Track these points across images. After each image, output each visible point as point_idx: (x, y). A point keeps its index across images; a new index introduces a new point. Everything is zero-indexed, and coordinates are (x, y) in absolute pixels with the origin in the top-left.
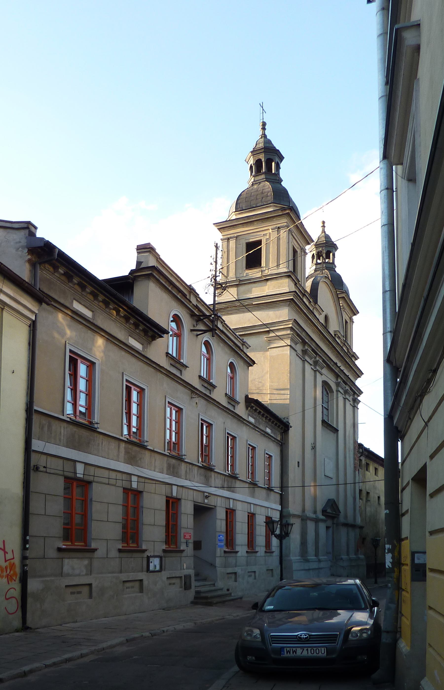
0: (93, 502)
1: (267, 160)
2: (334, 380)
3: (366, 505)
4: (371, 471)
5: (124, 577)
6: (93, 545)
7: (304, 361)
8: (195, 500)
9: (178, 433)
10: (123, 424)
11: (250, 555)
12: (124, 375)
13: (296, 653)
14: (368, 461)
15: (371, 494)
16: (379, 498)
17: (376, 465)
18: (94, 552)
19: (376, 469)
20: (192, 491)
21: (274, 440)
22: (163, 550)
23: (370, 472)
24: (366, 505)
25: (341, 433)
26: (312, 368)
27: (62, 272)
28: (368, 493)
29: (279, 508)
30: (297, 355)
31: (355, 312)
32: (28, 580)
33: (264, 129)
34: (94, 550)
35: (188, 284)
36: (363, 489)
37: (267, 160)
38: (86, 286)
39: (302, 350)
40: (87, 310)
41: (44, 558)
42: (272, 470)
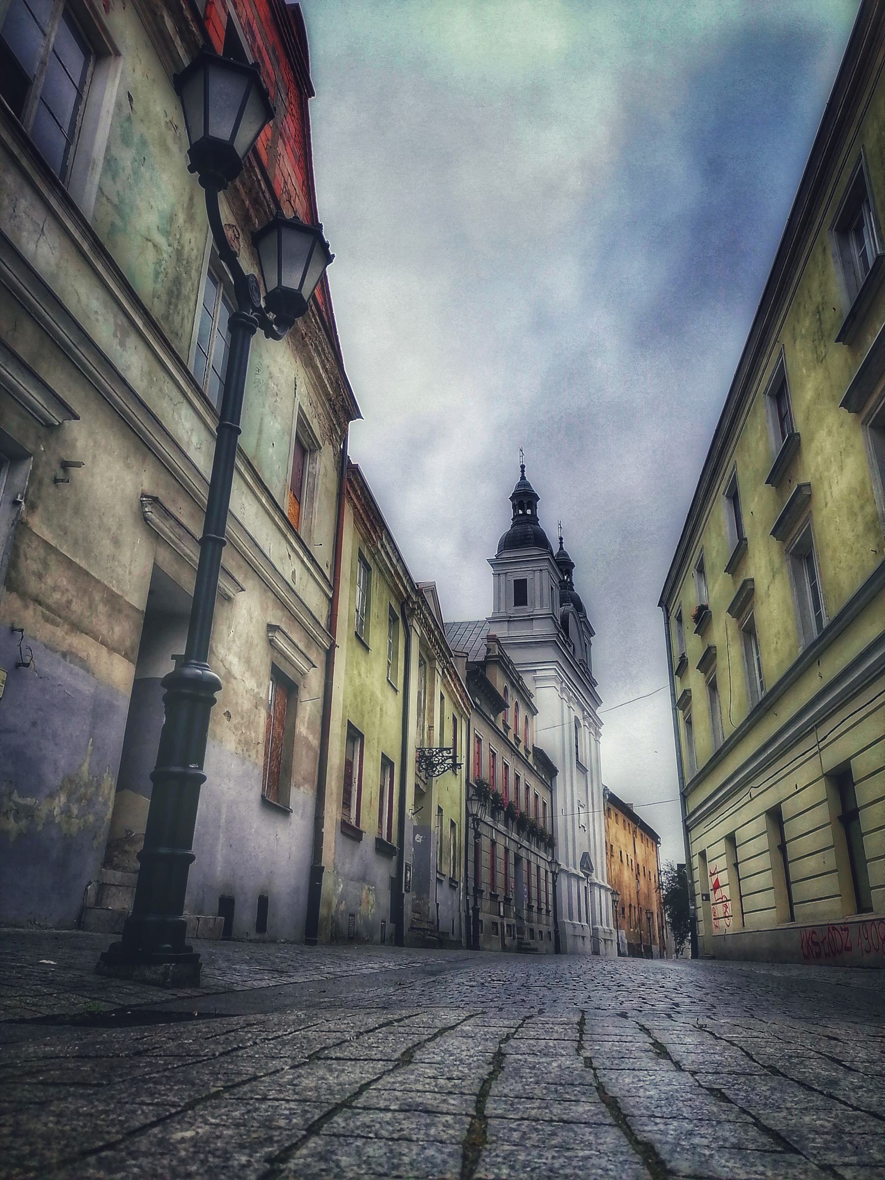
1: (524, 499)
21: (543, 782)
33: (523, 471)
37: (524, 499)
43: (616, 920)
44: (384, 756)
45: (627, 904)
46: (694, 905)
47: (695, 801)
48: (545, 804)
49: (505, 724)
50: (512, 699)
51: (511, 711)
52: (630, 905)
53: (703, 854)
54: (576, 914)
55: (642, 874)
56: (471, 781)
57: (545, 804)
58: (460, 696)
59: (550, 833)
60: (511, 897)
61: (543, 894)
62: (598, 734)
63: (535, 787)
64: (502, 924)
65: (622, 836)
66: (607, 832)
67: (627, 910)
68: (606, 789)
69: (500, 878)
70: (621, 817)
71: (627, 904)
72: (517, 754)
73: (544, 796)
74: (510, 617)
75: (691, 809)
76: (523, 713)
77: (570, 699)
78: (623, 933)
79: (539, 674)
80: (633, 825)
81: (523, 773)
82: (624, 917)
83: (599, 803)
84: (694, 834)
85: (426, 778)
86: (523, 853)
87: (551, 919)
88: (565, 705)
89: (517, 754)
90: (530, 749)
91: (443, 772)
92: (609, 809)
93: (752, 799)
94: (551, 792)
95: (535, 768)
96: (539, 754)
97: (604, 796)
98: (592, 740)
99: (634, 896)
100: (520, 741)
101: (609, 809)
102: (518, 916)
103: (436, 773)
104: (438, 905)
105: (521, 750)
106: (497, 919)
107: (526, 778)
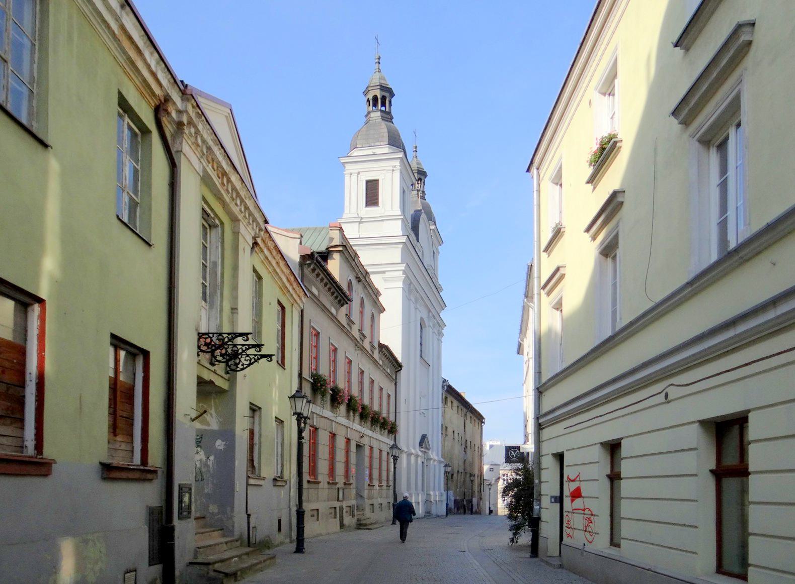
18: (319, 483)
21: (388, 376)
43: (447, 484)
44: (113, 336)
45: (456, 471)
46: (539, 505)
47: (553, 399)
48: (389, 396)
49: (348, 316)
50: (357, 293)
51: (356, 304)
52: (458, 471)
53: (560, 457)
54: (413, 486)
55: (469, 447)
56: (306, 375)
57: (389, 396)
58: (288, 280)
59: (393, 421)
60: (351, 481)
61: (384, 474)
62: (440, 334)
63: (381, 380)
64: (341, 509)
65: (454, 416)
66: (443, 416)
67: (455, 475)
68: (445, 381)
69: (340, 469)
70: (456, 403)
71: (456, 471)
72: (363, 349)
73: (388, 387)
74: (362, 218)
75: (546, 408)
76: (369, 308)
77: (416, 301)
78: (451, 493)
79: (387, 274)
80: (465, 410)
81: (368, 367)
82: (453, 481)
83: (439, 393)
84: (546, 433)
85: (227, 373)
86: (365, 441)
87: (391, 492)
88: (412, 306)
89: (363, 349)
90: (376, 345)
91: (249, 365)
92: (446, 398)
93: (669, 402)
94: (396, 384)
95: (381, 363)
96: (383, 348)
97: (443, 387)
98: (435, 339)
99: (461, 464)
100: (365, 337)
101: (446, 398)
102: (359, 496)
103: (240, 366)
104: (249, 516)
105: (367, 345)
106: (337, 504)
107: (371, 372)
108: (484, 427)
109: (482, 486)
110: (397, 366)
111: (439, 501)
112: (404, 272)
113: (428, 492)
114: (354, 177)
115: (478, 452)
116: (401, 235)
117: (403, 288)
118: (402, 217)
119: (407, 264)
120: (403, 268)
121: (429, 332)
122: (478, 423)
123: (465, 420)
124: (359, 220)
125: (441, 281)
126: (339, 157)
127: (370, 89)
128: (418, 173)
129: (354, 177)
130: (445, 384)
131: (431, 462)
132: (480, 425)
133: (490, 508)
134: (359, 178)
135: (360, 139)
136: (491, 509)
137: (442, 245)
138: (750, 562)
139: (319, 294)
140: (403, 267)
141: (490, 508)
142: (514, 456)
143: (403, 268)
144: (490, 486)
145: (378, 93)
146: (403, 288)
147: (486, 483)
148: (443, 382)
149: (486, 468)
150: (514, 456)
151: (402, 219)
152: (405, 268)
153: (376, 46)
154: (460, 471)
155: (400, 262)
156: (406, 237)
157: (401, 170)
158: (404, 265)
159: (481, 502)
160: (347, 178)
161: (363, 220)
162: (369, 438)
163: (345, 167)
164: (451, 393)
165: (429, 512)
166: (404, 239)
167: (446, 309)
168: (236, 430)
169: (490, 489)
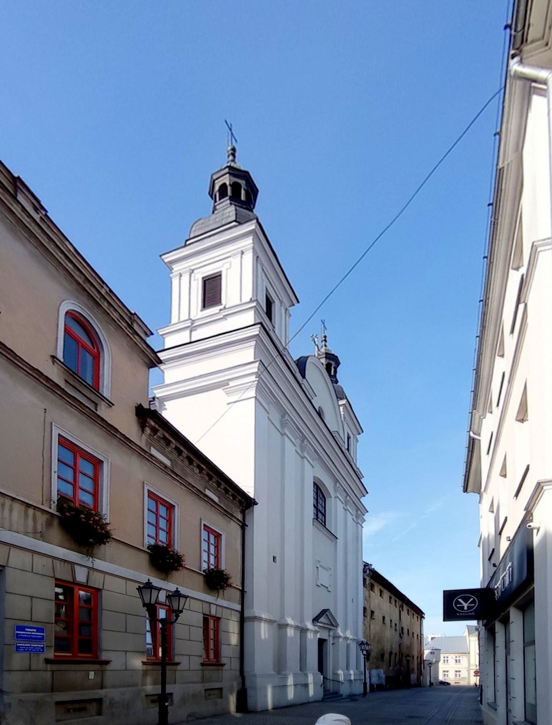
0: (104, 611)
2: (333, 484)
3: (370, 623)
4: (376, 591)
5: (208, 685)
6: (104, 656)
7: (283, 434)
8: (58, 576)
9: (217, 557)
10: (202, 561)
11: (205, 667)
12: (145, 485)
13: (447, 676)
14: (373, 582)
15: (376, 613)
16: (384, 618)
17: (382, 589)
18: (223, 666)
19: (381, 592)
20: (221, 608)
22: (201, 663)
23: (374, 592)
24: (370, 623)
25: (340, 542)
26: (296, 451)
27: (205, 473)
28: (372, 612)
29: (239, 608)
30: (269, 418)
31: (360, 431)
32: (167, 685)
34: (178, 664)
35: (16, 175)
36: (367, 607)
38: (193, 460)
39: (281, 421)
40: (165, 458)
41: (189, 670)
42: (221, 554)
65: (382, 604)
68: (366, 565)
80: (399, 603)
94: (243, 526)
97: (364, 572)
108: (425, 622)
109: (422, 665)
110: (246, 503)
111: (355, 680)
112: (258, 375)
113: (335, 672)
114: (185, 278)
115: (418, 639)
116: (252, 323)
117: (256, 397)
118: (254, 304)
119: (261, 361)
120: (256, 370)
121: (336, 507)
122: (418, 617)
123: (400, 611)
124: (189, 324)
125: (361, 465)
126: (161, 256)
127: (215, 177)
128: (326, 357)
129: (185, 278)
130: (367, 568)
131: (341, 640)
132: (419, 620)
133: (430, 681)
134: (192, 278)
135: (268, 366)
136: (432, 682)
137: (362, 434)
138: (103, 608)
139: (172, 464)
140: (254, 368)
141: (430, 681)
142: (466, 608)
143: (256, 370)
144: (430, 665)
145: (227, 180)
146: (256, 397)
147: (426, 663)
148: (365, 566)
149: (426, 652)
150: (466, 608)
151: (255, 307)
152: (258, 369)
153: (230, 138)
154: (394, 652)
155: (252, 360)
156: (259, 326)
157: (254, 248)
158: (257, 364)
159: (421, 677)
160: (175, 282)
161: (196, 324)
162: (208, 605)
163: (171, 269)
164: (375, 580)
165: (337, 692)
166: (256, 330)
167: (367, 495)
168: (288, 648)
169: (430, 667)
